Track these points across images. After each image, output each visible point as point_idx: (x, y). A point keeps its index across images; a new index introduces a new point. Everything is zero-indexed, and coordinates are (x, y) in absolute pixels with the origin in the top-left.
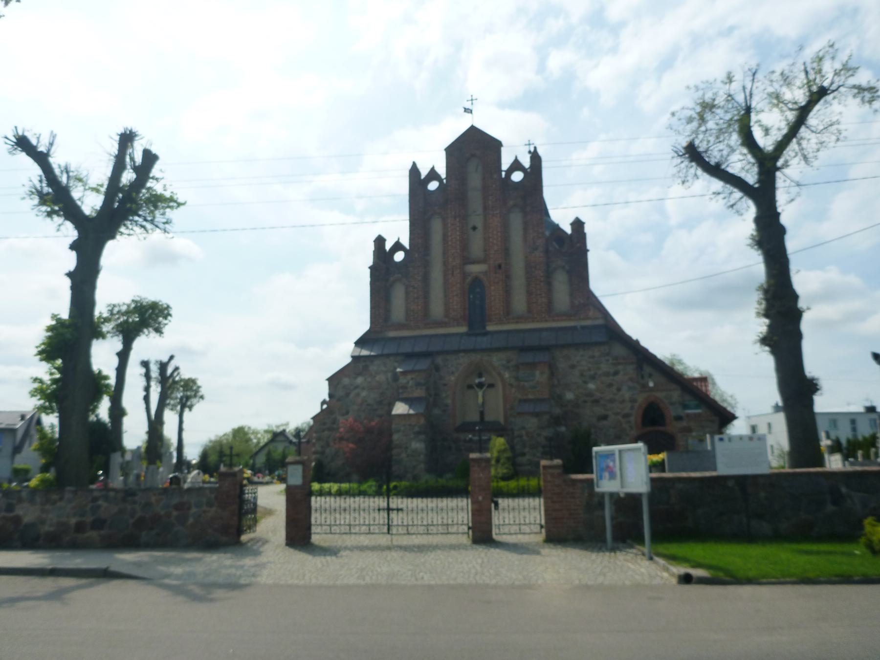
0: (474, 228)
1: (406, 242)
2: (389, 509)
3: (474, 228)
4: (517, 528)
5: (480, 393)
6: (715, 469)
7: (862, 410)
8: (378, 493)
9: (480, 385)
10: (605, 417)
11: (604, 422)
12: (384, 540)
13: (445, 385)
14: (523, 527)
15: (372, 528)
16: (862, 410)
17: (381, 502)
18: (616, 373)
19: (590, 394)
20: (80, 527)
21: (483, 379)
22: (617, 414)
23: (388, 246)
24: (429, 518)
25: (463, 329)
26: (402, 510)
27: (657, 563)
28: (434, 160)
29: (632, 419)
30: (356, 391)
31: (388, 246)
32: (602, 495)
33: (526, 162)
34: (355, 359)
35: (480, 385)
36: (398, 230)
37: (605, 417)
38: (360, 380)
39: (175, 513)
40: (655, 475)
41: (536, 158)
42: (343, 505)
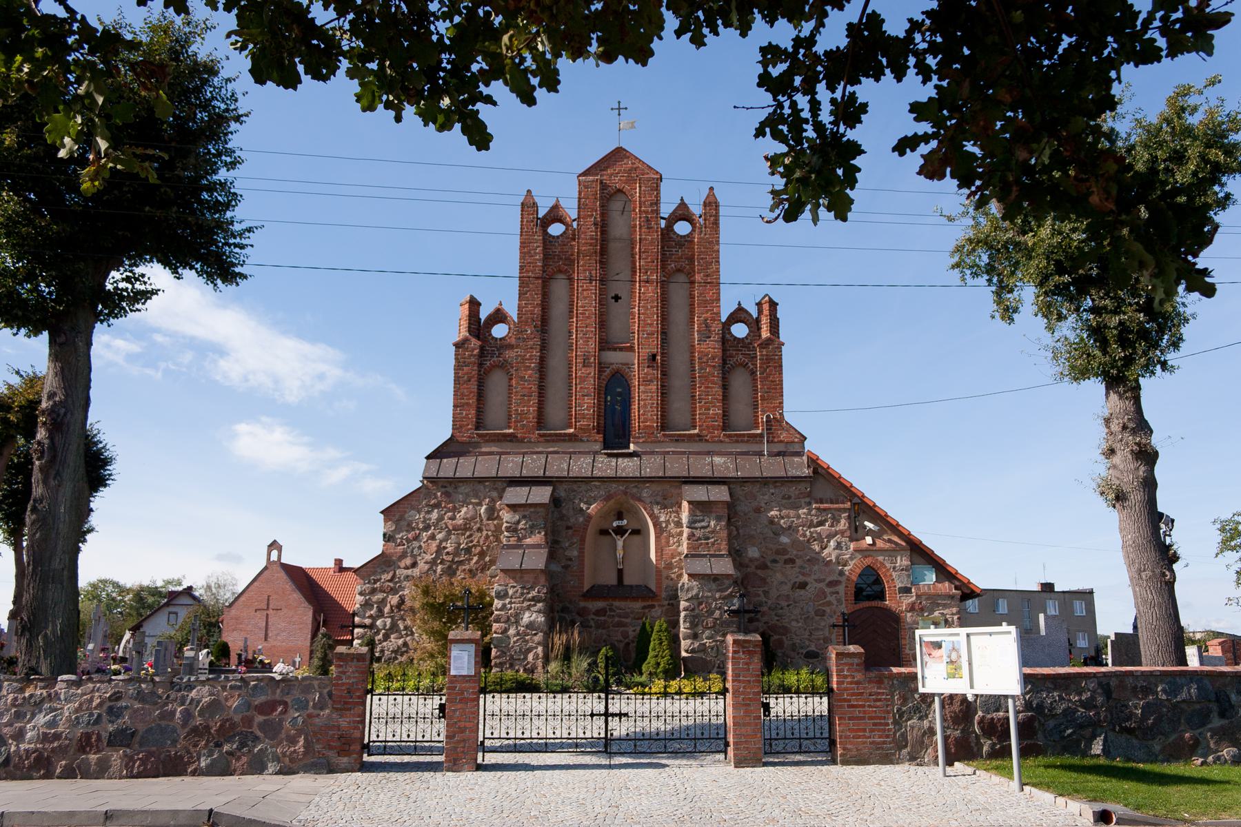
0: (617, 298)
1: (512, 311)
2: (607, 714)
3: (617, 298)
4: (796, 743)
5: (620, 543)
6: (1140, 665)
7: (1037, 588)
8: (593, 687)
9: (620, 531)
10: (803, 586)
11: (802, 592)
12: (605, 762)
13: (568, 528)
14: (805, 743)
15: (774, 743)
16: (1037, 588)
17: (595, 703)
18: (821, 523)
19: (784, 551)
20: (85, 743)
21: (625, 522)
22: (819, 581)
23: (484, 314)
24: (384, 706)
26: (626, 715)
27: (527, 750)
28: (562, 191)
29: (841, 589)
31: (484, 314)
32: (928, 699)
33: (696, 210)
34: (431, 481)
35: (620, 531)
36: (503, 294)
37: (803, 586)
39: (260, 718)
40: (1028, 671)
41: (711, 204)
42: (566, 708)
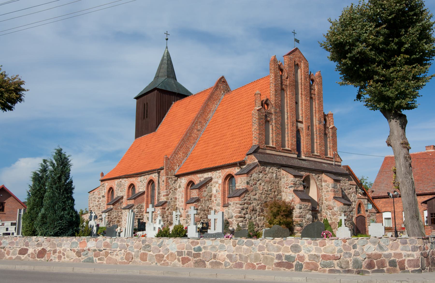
25: (295, 156)
30: (260, 182)
38: (261, 175)
